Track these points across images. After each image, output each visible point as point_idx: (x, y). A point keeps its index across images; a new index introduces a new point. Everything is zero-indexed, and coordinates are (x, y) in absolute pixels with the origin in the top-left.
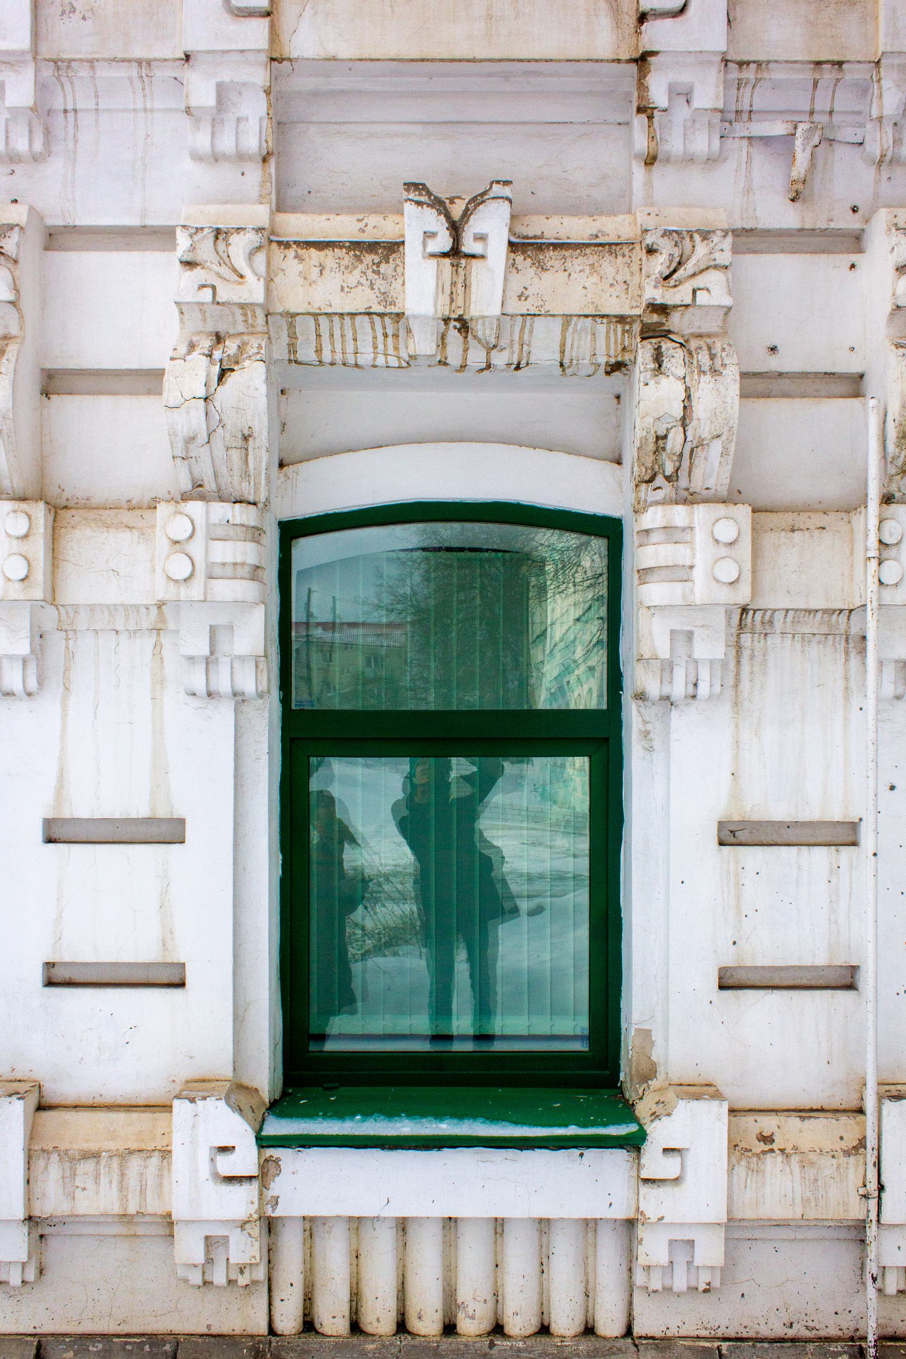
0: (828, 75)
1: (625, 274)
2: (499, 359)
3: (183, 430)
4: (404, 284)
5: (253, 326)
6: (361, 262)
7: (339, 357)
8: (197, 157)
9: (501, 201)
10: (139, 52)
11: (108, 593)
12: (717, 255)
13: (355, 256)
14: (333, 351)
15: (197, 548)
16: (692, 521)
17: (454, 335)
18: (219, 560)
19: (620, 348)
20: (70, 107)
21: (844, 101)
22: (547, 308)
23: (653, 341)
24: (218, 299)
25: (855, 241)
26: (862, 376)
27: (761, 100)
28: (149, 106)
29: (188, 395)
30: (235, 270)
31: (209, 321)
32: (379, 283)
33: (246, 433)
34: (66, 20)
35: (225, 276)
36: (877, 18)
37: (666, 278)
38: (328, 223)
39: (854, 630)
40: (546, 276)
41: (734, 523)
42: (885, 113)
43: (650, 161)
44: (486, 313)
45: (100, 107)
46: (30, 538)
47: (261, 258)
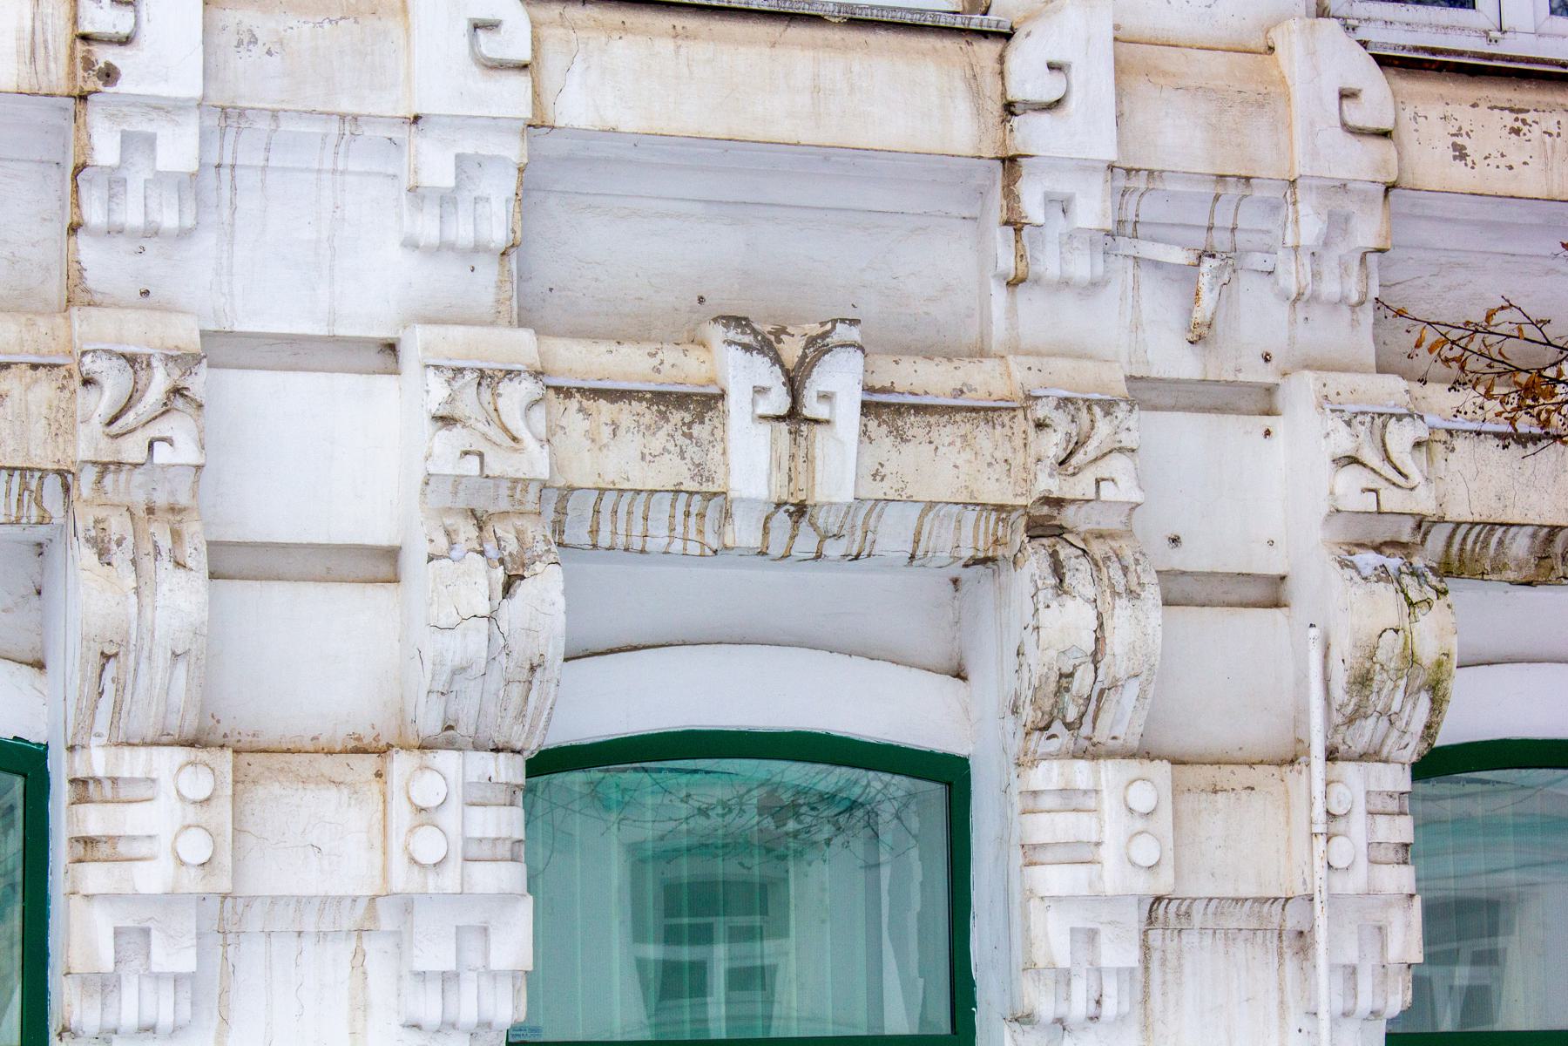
0: (1233, 191)
1: (1005, 451)
2: (833, 549)
3: (454, 659)
4: (724, 453)
5: (521, 503)
6: (668, 421)
7: (621, 541)
8: (411, 244)
9: (851, 350)
10: (346, 106)
11: (309, 880)
12: (1123, 436)
13: (659, 411)
14: (614, 533)
15: (450, 819)
16: (1097, 780)
17: (782, 520)
18: (477, 834)
19: (991, 539)
20: (228, 160)
21: (1249, 218)
22: (909, 492)
23: (1045, 541)
24: (487, 472)
25: (1265, 402)
26: (1283, 578)
27: (1151, 209)
28: (341, 167)
29: (466, 613)
30: (506, 430)
31: (461, 494)
32: (691, 450)
33: (536, 662)
34: (244, 53)
35: (494, 438)
36: (1290, 126)
37: (1061, 463)
38: (609, 356)
39: (1291, 924)
40: (907, 449)
41: (1150, 786)
42: (1302, 243)
43: (1014, 283)
44: (834, 500)
45: (271, 164)
46: (213, 803)
47: (539, 414)
